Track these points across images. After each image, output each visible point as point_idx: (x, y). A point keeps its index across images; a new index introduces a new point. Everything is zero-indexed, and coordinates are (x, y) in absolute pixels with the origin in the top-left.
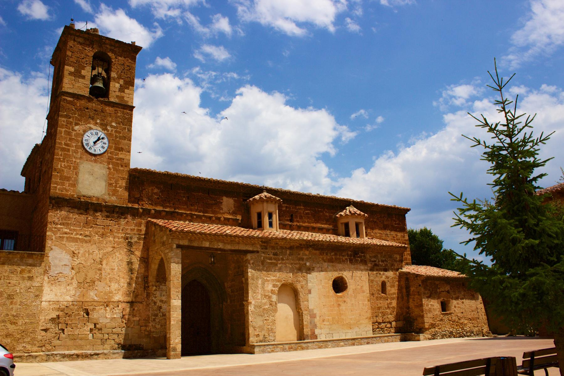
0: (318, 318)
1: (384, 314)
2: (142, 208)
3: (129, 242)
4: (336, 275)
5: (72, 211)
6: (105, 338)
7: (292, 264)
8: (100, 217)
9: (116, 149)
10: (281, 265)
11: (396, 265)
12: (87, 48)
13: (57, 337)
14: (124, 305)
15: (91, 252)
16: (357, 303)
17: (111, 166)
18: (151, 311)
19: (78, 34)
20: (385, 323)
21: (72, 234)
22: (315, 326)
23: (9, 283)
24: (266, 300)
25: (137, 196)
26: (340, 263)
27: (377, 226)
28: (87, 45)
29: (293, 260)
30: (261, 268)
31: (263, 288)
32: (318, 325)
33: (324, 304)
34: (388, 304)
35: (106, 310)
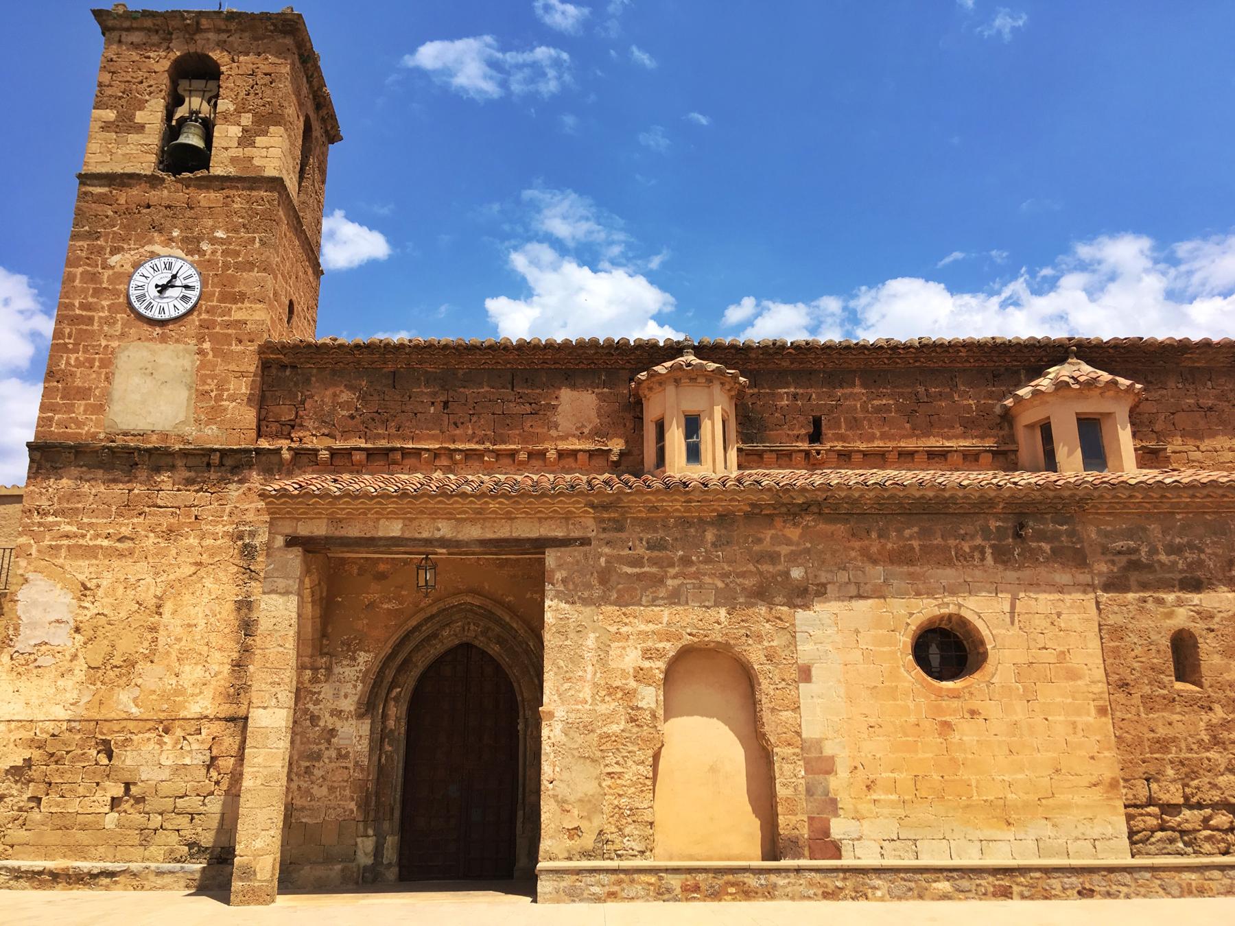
0: (843, 773)
1: (1189, 772)
2: (290, 449)
3: (245, 546)
4: (927, 609)
5: (88, 477)
6: (152, 825)
7: (724, 576)
8: (167, 486)
9: (223, 299)
10: (677, 582)
12: (152, 55)
13: (20, 821)
14: (217, 728)
15: (133, 580)
16: (1039, 719)
17: (207, 345)
19: (127, 24)
20: (1200, 806)
21: (83, 536)
22: (832, 805)
25: (287, 416)
26: (949, 563)
27: (1222, 422)
28: (153, 45)
29: (730, 562)
30: (597, 593)
31: (602, 661)
32: (845, 801)
33: (872, 721)
34: (1210, 727)
35: (161, 743)
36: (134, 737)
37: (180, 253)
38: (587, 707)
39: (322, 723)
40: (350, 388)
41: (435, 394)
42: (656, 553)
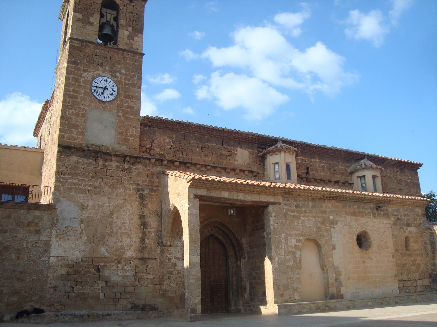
1: (409, 271)
3: (141, 194)
7: (315, 217)
9: (125, 97)
11: (418, 219)
13: (67, 296)
15: (101, 204)
18: (165, 269)
21: (81, 185)
22: (341, 284)
23: (16, 237)
24: (290, 257)
26: (363, 216)
31: (286, 243)
36: (108, 264)
37: (108, 76)
38: (283, 257)
39: (172, 261)
40: (169, 137)
41: (198, 144)
42: (298, 209)
